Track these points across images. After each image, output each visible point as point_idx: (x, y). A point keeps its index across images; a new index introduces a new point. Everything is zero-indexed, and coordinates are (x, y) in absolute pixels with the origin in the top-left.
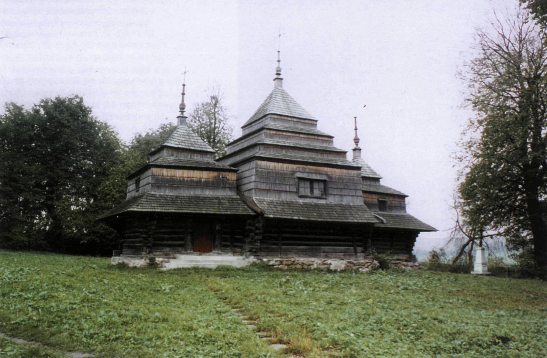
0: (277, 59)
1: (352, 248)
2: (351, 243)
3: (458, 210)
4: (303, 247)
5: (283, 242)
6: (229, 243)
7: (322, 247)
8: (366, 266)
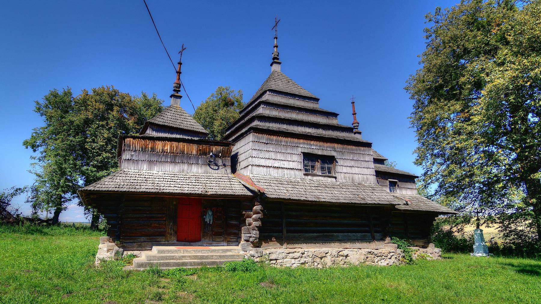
0: (179, 62)
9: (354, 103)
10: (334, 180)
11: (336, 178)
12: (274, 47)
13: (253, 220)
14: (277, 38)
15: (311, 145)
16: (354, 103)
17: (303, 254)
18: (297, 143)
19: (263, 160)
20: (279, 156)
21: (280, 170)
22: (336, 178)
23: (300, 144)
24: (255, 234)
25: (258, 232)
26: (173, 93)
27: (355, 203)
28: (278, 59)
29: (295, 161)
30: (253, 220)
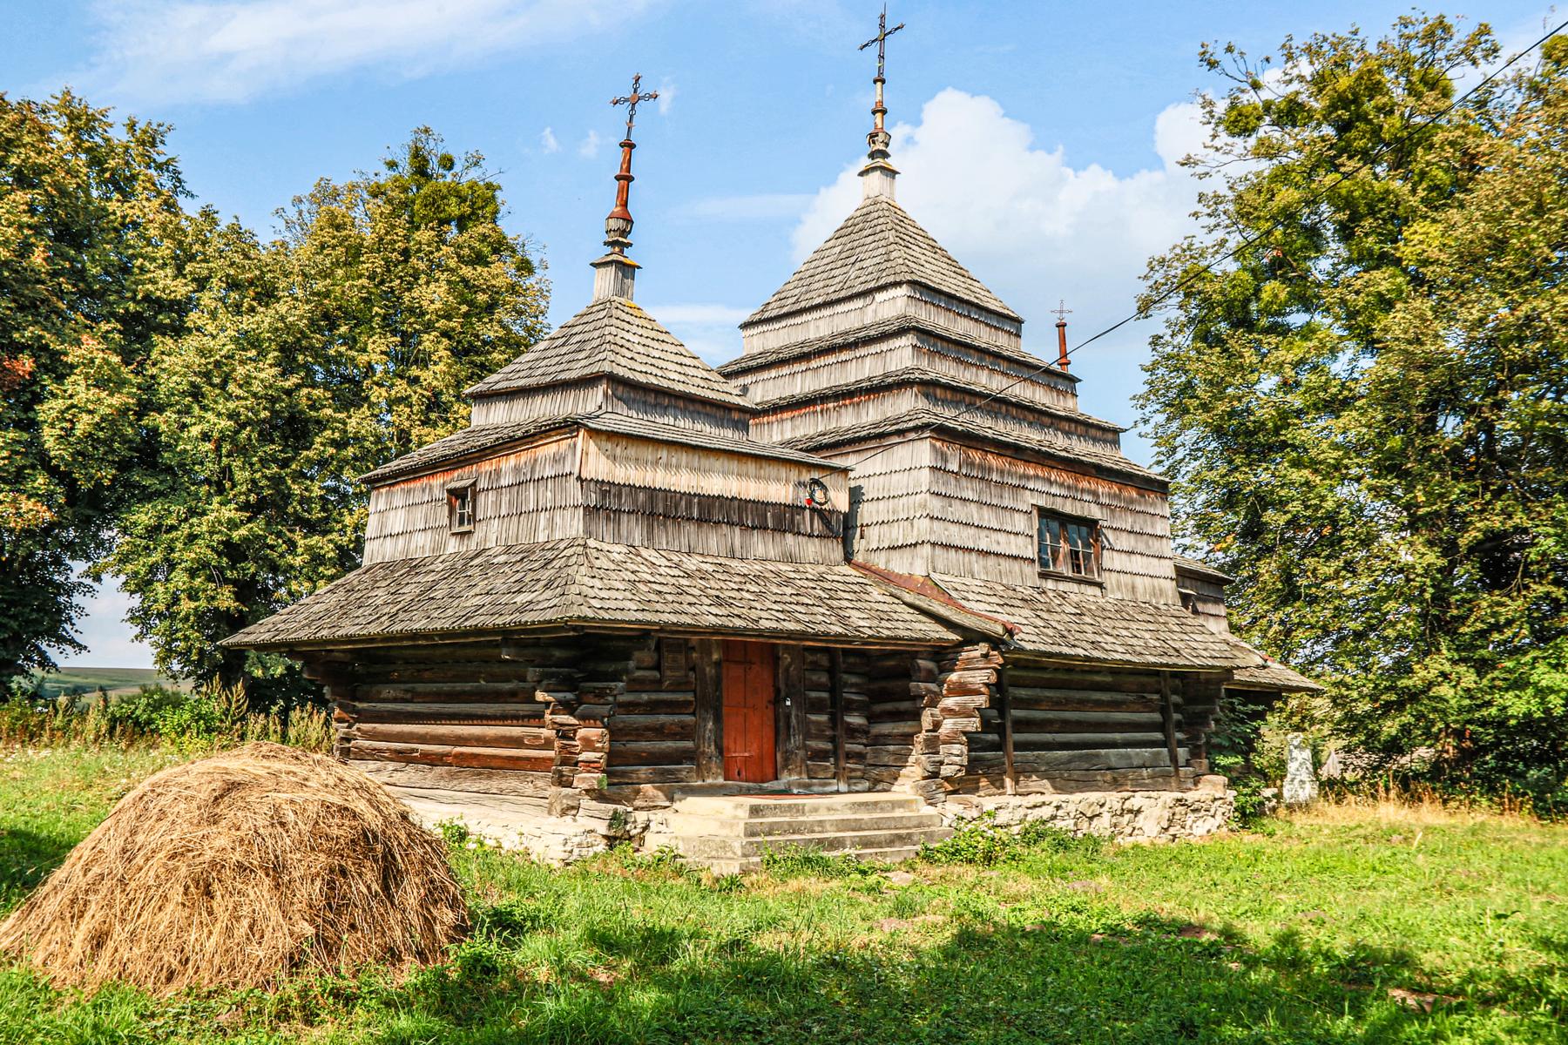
0: (623, 139)
1: (1165, 750)
2: (1159, 736)
3: (1000, 630)
7: (1103, 751)
9: (1064, 325)
10: (1097, 591)
11: (1100, 585)
12: (874, 112)
13: (952, 715)
14: (883, 82)
15: (1051, 483)
16: (1064, 325)
17: (1058, 808)
18: (1022, 477)
19: (954, 529)
20: (988, 518)
21: (992, 561)
22: (1100, 585)
23: (1028, 478)
24: (954, 757)
25: (965, 749)
26: (602, 253)
27: (415, 635)
28: (885, 155)
29: (1019, 536)
30: (952, 715)
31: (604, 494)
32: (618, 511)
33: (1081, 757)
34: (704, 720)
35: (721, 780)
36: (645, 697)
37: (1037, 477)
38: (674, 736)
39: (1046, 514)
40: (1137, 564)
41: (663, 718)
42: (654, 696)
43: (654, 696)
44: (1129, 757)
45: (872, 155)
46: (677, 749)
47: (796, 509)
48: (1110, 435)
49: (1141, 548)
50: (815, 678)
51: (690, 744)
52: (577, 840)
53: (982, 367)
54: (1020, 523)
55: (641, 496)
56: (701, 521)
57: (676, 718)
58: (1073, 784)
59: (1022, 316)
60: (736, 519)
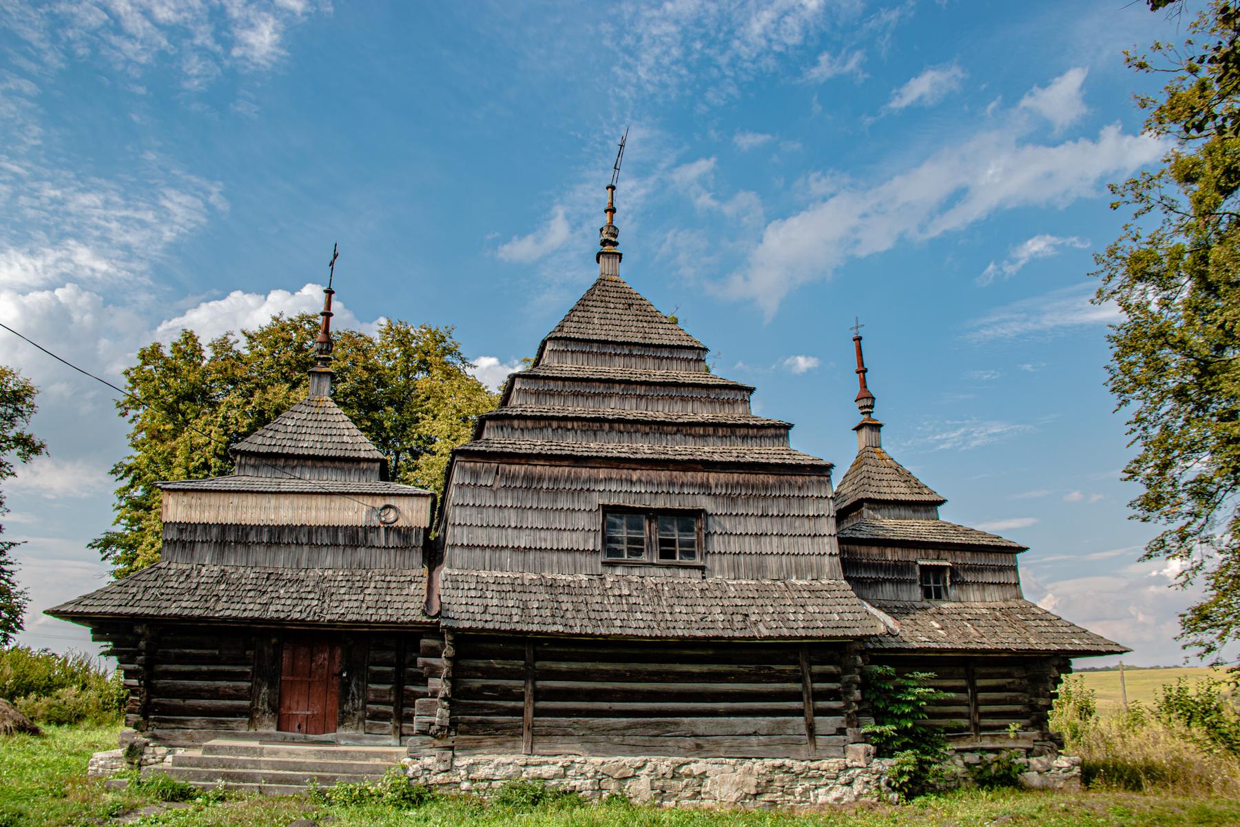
4: (612, 720)
5: (821, 704)
6: (391, 709)
8: (842, 779)
10: (698, 574)
18: (589, 480)
23: (597, 481)
31: (181, 531)
32: (193, 543)
33: (645, 725)
34: (260, 686)
35: (273, 730)
36: (204, 668)
37: (609, 480)
38: (230, 697)
39: (607, 510)
40: (735, 545)
41: (222, 684)
42: (213, 668)
43: (213, 668)
44: (732, 725)
45: (604, 243)
46: (231, 707)
47: (368, 529)
48: (781, 430)
49: (495, 533)
50: (880, 670)
51: (247, 703)
52: (101, 763)
53: (611, 395)
54: (583, 521)
55: (215, 531)
56: (269, 544)
57: (231, 684)
58: (626, 748)
59: (701, 339)
60: (305, 540)
